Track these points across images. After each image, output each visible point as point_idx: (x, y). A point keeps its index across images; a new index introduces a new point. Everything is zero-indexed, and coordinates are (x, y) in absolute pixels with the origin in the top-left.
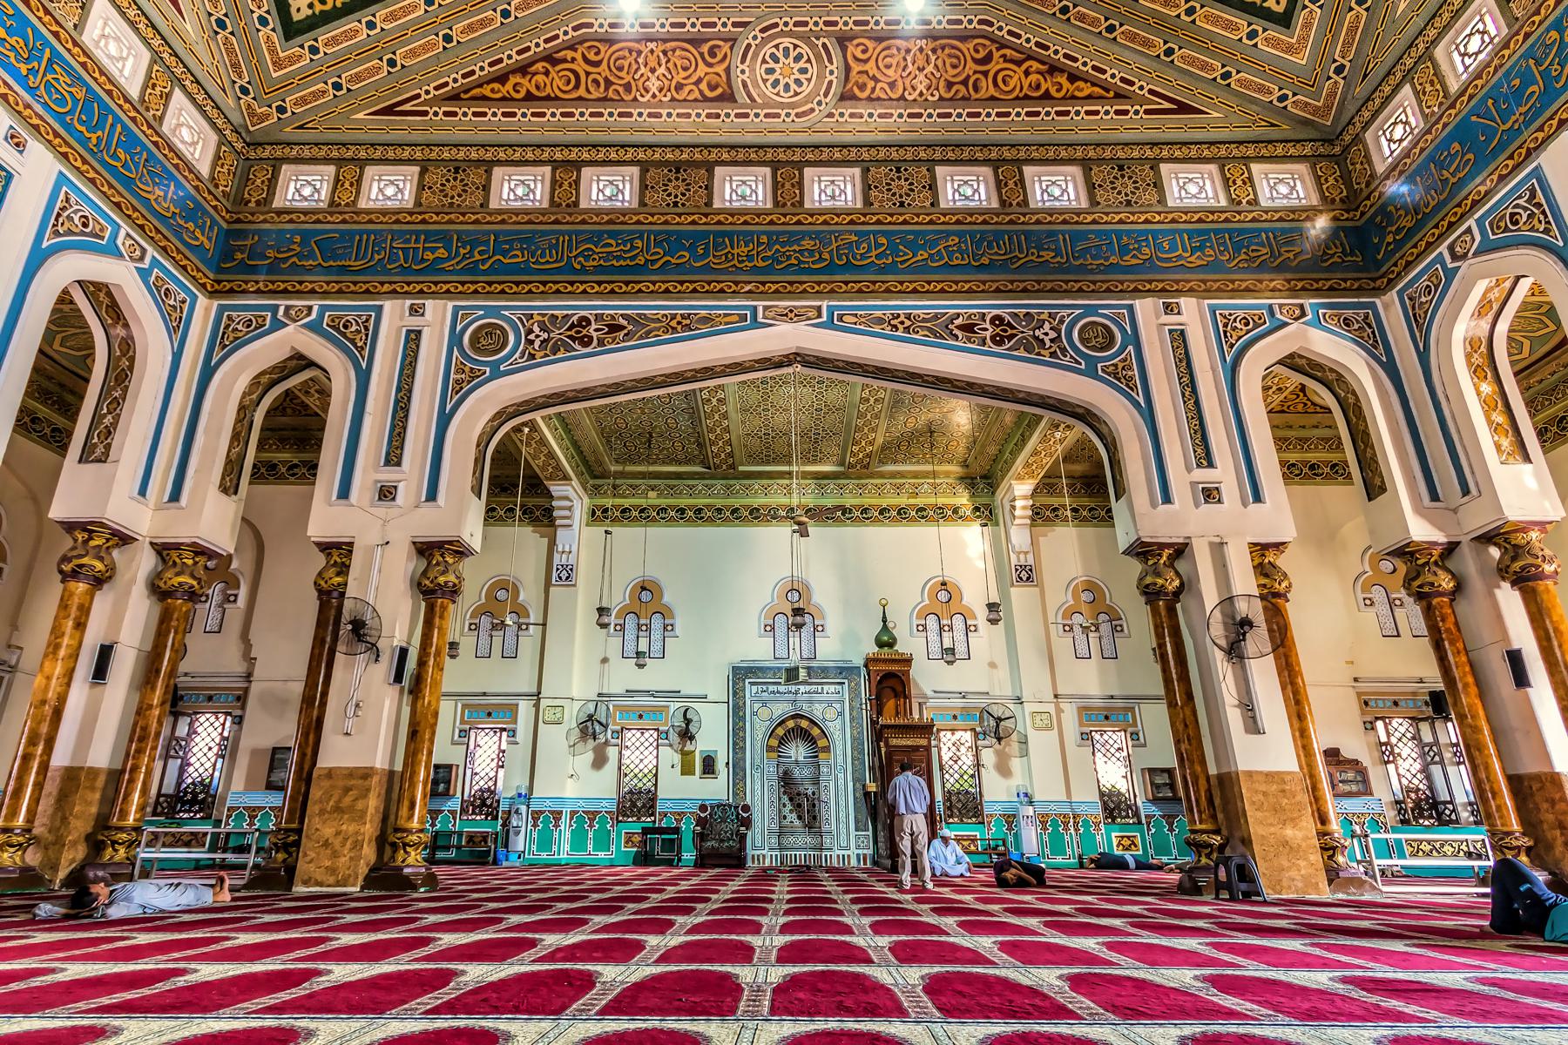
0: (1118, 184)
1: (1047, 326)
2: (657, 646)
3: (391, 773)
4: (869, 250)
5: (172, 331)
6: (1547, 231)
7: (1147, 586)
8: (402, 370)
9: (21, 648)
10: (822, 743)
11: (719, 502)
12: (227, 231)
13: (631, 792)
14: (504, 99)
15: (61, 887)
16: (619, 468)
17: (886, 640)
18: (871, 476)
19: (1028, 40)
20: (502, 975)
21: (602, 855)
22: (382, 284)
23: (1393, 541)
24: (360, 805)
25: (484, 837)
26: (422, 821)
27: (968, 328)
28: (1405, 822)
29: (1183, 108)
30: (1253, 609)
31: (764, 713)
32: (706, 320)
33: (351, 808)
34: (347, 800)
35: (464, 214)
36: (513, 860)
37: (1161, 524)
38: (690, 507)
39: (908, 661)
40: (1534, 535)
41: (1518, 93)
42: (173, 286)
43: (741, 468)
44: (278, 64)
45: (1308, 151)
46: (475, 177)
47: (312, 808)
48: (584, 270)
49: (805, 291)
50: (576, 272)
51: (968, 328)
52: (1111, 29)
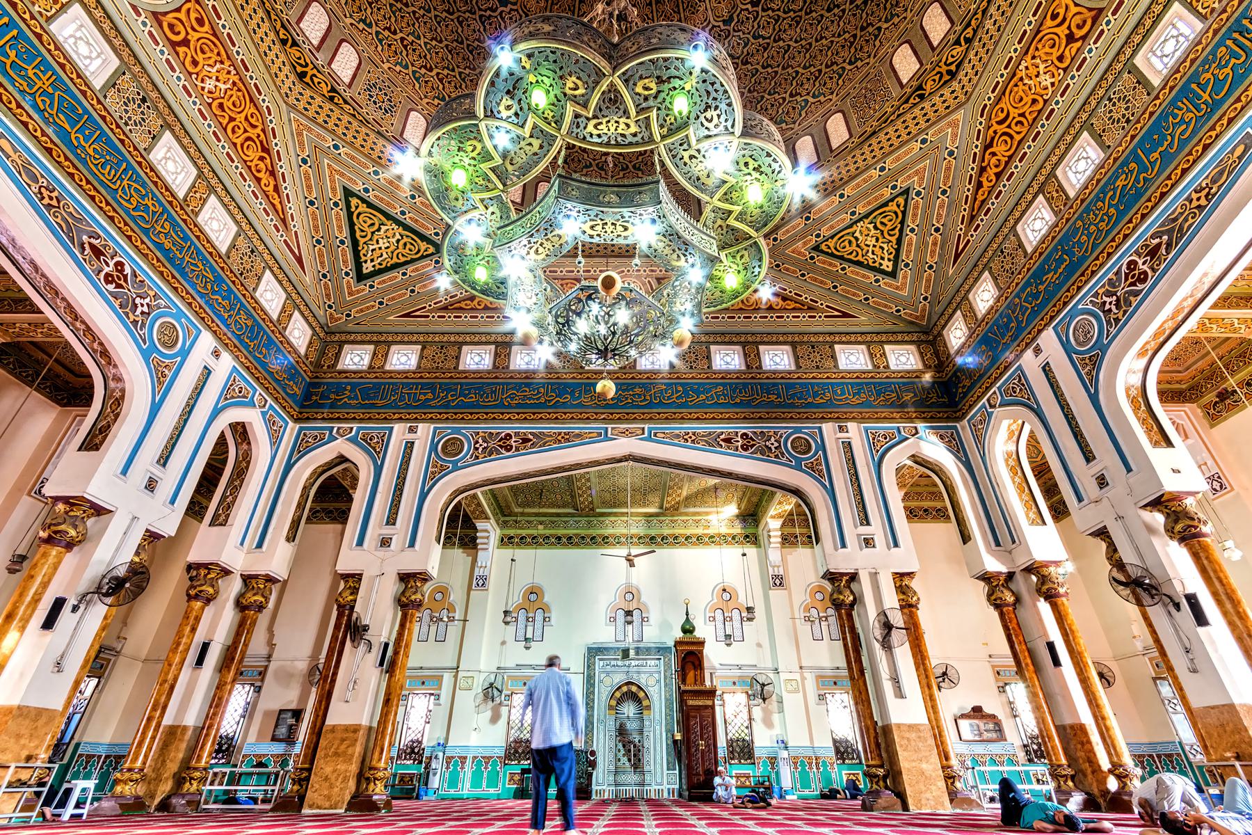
0: (811, 356)
1: (773, 439)
2: (538, 633)
3: (370, 728)
4: (672, 394)
5: (272, 444)
6: (1029, 399)
7: (834, 600)
8: (401, 465)
9: (125, 639)
10: (645, 703)
11: (583, 532)
12: (310, 383)
13: (515, 741)
14: (472, 309)
15: (156, 810)
16: (520, 510)
17: (688, 629)
18: (681, 514)
21: (492, 791)
22: (394, 414)
23: (978, 571)
24: (350, 751)
25: (412, 776)
26: (386, 763)
27: (728, 441)
28: (1030, 761)
29: (845, 315)
30: (897, 619)
31: (608, 681)
32: (578, 436)
33: (345, 753)
34: (343, 747)
35: (444, 373)
36: (431, 796)
37: (843, 562)
38: (564, 536)
39: (702, 643)
40: (1052, 569)
41: (1007, 325)
42: (277, 419)
43: (598, 510)
44: (350, 294)
45: (915, 338)
46: (452, 351)
47: (320, 753)
48: (510, 406)
49: (635, 418)
50: (503, 406)
51: (728, 441)
52: (803, 275)
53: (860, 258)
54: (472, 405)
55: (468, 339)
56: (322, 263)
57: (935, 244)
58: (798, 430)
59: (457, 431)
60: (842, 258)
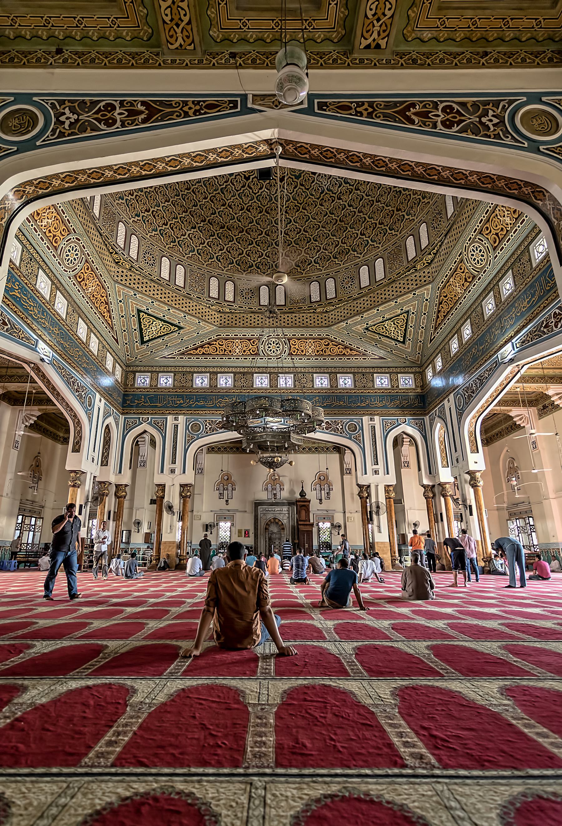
19: (339, 340)
37: (363, 481)
39: (309, 501)
48: (220, 407)
50: (218, 408)
51: (424, 115)
57: (422, 332)
58: (352, 420)
60: (379, 334)
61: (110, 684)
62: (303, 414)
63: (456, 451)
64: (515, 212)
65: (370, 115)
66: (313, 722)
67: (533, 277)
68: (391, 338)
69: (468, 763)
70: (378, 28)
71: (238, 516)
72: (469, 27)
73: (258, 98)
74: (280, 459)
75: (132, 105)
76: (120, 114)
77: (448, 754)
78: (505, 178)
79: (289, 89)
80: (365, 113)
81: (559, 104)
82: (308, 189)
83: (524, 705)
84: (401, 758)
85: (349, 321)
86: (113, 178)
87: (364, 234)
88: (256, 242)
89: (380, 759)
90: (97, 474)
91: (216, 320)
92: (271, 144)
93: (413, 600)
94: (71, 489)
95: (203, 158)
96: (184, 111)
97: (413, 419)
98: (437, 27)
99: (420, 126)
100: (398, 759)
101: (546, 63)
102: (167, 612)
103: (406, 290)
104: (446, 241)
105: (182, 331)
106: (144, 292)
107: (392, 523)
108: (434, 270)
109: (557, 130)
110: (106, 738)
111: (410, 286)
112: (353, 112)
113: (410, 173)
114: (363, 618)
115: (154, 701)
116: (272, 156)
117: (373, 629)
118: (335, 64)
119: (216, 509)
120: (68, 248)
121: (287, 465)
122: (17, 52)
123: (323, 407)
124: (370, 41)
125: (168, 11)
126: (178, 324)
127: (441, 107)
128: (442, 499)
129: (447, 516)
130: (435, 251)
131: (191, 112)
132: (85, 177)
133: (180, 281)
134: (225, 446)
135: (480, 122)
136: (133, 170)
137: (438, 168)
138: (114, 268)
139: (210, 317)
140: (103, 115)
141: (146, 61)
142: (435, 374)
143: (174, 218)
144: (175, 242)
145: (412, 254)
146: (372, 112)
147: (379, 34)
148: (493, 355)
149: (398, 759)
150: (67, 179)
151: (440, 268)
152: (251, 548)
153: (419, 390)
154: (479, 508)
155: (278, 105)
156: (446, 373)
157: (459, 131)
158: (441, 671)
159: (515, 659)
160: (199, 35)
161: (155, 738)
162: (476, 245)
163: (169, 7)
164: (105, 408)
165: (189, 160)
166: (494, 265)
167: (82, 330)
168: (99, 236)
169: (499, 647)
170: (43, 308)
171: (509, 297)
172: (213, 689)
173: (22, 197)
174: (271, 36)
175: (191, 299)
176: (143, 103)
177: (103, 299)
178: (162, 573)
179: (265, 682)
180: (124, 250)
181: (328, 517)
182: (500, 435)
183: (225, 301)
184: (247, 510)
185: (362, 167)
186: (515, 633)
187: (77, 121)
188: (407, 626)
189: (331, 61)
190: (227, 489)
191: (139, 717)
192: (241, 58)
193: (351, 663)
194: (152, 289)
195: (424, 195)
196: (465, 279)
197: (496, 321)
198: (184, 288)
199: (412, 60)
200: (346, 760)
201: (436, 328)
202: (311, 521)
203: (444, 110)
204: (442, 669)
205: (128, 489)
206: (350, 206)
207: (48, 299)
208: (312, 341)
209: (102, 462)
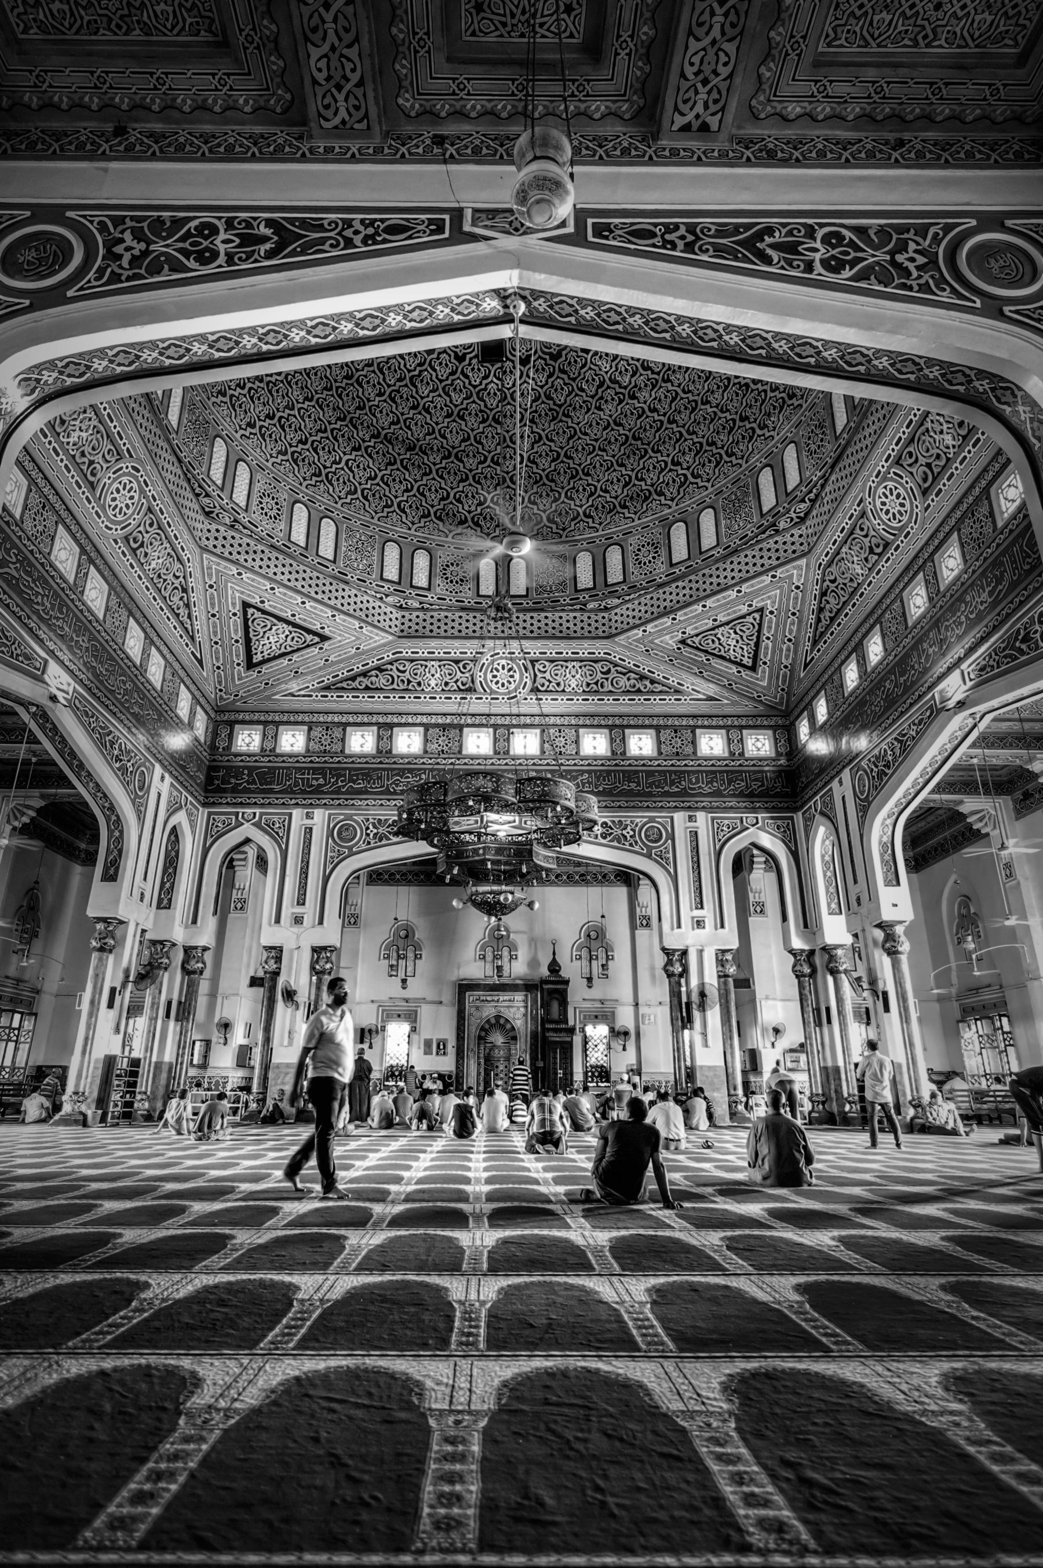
20: (153, 1237)
37: (674, 940)
39: (567, 982)
46: (337, 733)
48: (395, 793)
50: (391, 794)
51: (791, 248)
53: (722, 653)
54: (360, 792)
55: (351, 720)
56: (217, 659)
57: (788, 650)
59: (349, 817)
60: (706, 651)
61: (148, 1366)
62: (559, 808)
63: (856, 882)
64: (961, 424)
65: (689, 247)
66: (560, 1450)
67: (998, 545)
68: (730, 661)
69: (876, 1541)
70: (705, 96)
71: (425, 1013)
72: (869, 97)
73: (484, 216)
74: (510, 897)
75: (249, 226)
76: (225, 242)
77: (836, 1521)
78: (941, 363)
79: (538, 202)
80: (680, 244)
81: (1037, 233)
82: (574, 380)
83: (990, 1413)
84: (740, 1530)
85: (649, 628)
86: (206, 358)
87: (679, 464)
88: (474, 477)
89: (697, 1534)
90: (148, 925)
91: (393, 624)
92: (506, 298)
93: (772, 1186)
94: (95, 955)
95: (378, 322)
96: (344, 237)
97: (772, 818)
98: (812, 96)
99: (782, 268)
100: (732, 1533)
101: (1010, 160)
102: (275, 1211)
103: (759, 568)
104: (833, 478)
105: (326, 645)
106: (257, 568)
107: (730, 1026)
108: (810, 531)
109: (1034, 279)
110: (133, 1486)
111: (765, 561)
112: (657, 241)
113: (763, 352)
114: (669, 1227)
115: (237, 1405)
116: (508, 319)
117: (687, 1249)
118: (626, 156)
119: (383, 996)
120: (115, 485)
121: (523, 908)
122: (42, 132)
123: (597, 794)
124: (690, 117)
125: (323, 64)
126: (321, 631)
127: (820, 234)
128: (830, 979)
129: (840, 1013)
130: (812, 496)
131: (357, 240)
132: (155, 354)
133: (327, 549)
134: (404, 869)
135: (893, 263)
136: (245, 342)
137: (815, 343)
138: (201, 524)
139: (381, 618)
140: (194, 244)
141: (279, 149)
142: (812, 733)
143: (320, 431)
144: (320, 475)
145: (769, 499)
146: (693, 243)
147: (706, 107)
148: (925, 693)
149: (732, 1533)
150: (120, 359)
151: (821, 527)
152: (450, 1077)
153: (783, 761)
154: (902, 997)
155: (518, 229)
156: (835, 728)
157: (855, 278)
158: (824, 1340)
159: (975, 1313)
160: (377, 104)
161: (234, 1485)
162: (891, 484)
163: (326, 56)
164: (171, 794)
165: (350, 326)
166: (924, 523)
167: (134, 643)
168: (176, 464)
169: (943, 1288)
170: (62, 600)
171: (954, 583)
172: (358, 1377)
173: (33, 391)
174: (509, 107)
175: (347, 583)
176: (270, 223)
177: (177, 583)
178: (270, 1131)
179: (464, 1364)
180: (222, 489)
181: (604, 1015)
182: (942, 851)
183: (412, 586)
184: (443, 999)
185: (675, 341)
186: (975, 1258)
187: (145, 253)
188: (758, 1242)
189: (618, 152)
190: (405, 957)
191: (202, 1439)
192: (452, 145)
193: (643, 1325)
194: (272, 564)
195: (791, 392)
196: (871, 548)
197: (930, 630)
198: (334, 562)
199: (768, 152)
200: (627, 1536)
201: (815, 642)
202: (571, 1023)
203: (826, 240)
204: (826, 1335)
205: (208, 957)
206: (654, 410)
207: (71, 580)
208: (577, 665)
209: (160, 901)
